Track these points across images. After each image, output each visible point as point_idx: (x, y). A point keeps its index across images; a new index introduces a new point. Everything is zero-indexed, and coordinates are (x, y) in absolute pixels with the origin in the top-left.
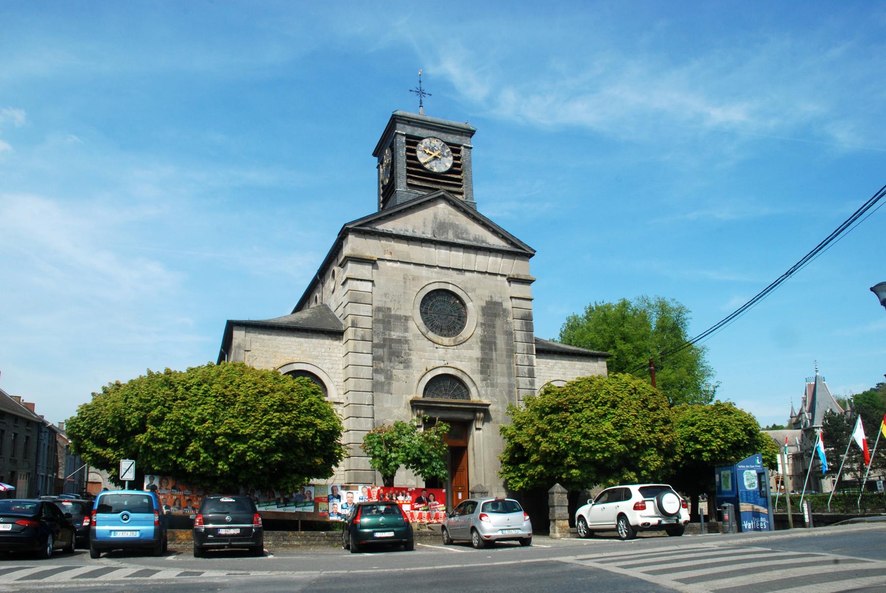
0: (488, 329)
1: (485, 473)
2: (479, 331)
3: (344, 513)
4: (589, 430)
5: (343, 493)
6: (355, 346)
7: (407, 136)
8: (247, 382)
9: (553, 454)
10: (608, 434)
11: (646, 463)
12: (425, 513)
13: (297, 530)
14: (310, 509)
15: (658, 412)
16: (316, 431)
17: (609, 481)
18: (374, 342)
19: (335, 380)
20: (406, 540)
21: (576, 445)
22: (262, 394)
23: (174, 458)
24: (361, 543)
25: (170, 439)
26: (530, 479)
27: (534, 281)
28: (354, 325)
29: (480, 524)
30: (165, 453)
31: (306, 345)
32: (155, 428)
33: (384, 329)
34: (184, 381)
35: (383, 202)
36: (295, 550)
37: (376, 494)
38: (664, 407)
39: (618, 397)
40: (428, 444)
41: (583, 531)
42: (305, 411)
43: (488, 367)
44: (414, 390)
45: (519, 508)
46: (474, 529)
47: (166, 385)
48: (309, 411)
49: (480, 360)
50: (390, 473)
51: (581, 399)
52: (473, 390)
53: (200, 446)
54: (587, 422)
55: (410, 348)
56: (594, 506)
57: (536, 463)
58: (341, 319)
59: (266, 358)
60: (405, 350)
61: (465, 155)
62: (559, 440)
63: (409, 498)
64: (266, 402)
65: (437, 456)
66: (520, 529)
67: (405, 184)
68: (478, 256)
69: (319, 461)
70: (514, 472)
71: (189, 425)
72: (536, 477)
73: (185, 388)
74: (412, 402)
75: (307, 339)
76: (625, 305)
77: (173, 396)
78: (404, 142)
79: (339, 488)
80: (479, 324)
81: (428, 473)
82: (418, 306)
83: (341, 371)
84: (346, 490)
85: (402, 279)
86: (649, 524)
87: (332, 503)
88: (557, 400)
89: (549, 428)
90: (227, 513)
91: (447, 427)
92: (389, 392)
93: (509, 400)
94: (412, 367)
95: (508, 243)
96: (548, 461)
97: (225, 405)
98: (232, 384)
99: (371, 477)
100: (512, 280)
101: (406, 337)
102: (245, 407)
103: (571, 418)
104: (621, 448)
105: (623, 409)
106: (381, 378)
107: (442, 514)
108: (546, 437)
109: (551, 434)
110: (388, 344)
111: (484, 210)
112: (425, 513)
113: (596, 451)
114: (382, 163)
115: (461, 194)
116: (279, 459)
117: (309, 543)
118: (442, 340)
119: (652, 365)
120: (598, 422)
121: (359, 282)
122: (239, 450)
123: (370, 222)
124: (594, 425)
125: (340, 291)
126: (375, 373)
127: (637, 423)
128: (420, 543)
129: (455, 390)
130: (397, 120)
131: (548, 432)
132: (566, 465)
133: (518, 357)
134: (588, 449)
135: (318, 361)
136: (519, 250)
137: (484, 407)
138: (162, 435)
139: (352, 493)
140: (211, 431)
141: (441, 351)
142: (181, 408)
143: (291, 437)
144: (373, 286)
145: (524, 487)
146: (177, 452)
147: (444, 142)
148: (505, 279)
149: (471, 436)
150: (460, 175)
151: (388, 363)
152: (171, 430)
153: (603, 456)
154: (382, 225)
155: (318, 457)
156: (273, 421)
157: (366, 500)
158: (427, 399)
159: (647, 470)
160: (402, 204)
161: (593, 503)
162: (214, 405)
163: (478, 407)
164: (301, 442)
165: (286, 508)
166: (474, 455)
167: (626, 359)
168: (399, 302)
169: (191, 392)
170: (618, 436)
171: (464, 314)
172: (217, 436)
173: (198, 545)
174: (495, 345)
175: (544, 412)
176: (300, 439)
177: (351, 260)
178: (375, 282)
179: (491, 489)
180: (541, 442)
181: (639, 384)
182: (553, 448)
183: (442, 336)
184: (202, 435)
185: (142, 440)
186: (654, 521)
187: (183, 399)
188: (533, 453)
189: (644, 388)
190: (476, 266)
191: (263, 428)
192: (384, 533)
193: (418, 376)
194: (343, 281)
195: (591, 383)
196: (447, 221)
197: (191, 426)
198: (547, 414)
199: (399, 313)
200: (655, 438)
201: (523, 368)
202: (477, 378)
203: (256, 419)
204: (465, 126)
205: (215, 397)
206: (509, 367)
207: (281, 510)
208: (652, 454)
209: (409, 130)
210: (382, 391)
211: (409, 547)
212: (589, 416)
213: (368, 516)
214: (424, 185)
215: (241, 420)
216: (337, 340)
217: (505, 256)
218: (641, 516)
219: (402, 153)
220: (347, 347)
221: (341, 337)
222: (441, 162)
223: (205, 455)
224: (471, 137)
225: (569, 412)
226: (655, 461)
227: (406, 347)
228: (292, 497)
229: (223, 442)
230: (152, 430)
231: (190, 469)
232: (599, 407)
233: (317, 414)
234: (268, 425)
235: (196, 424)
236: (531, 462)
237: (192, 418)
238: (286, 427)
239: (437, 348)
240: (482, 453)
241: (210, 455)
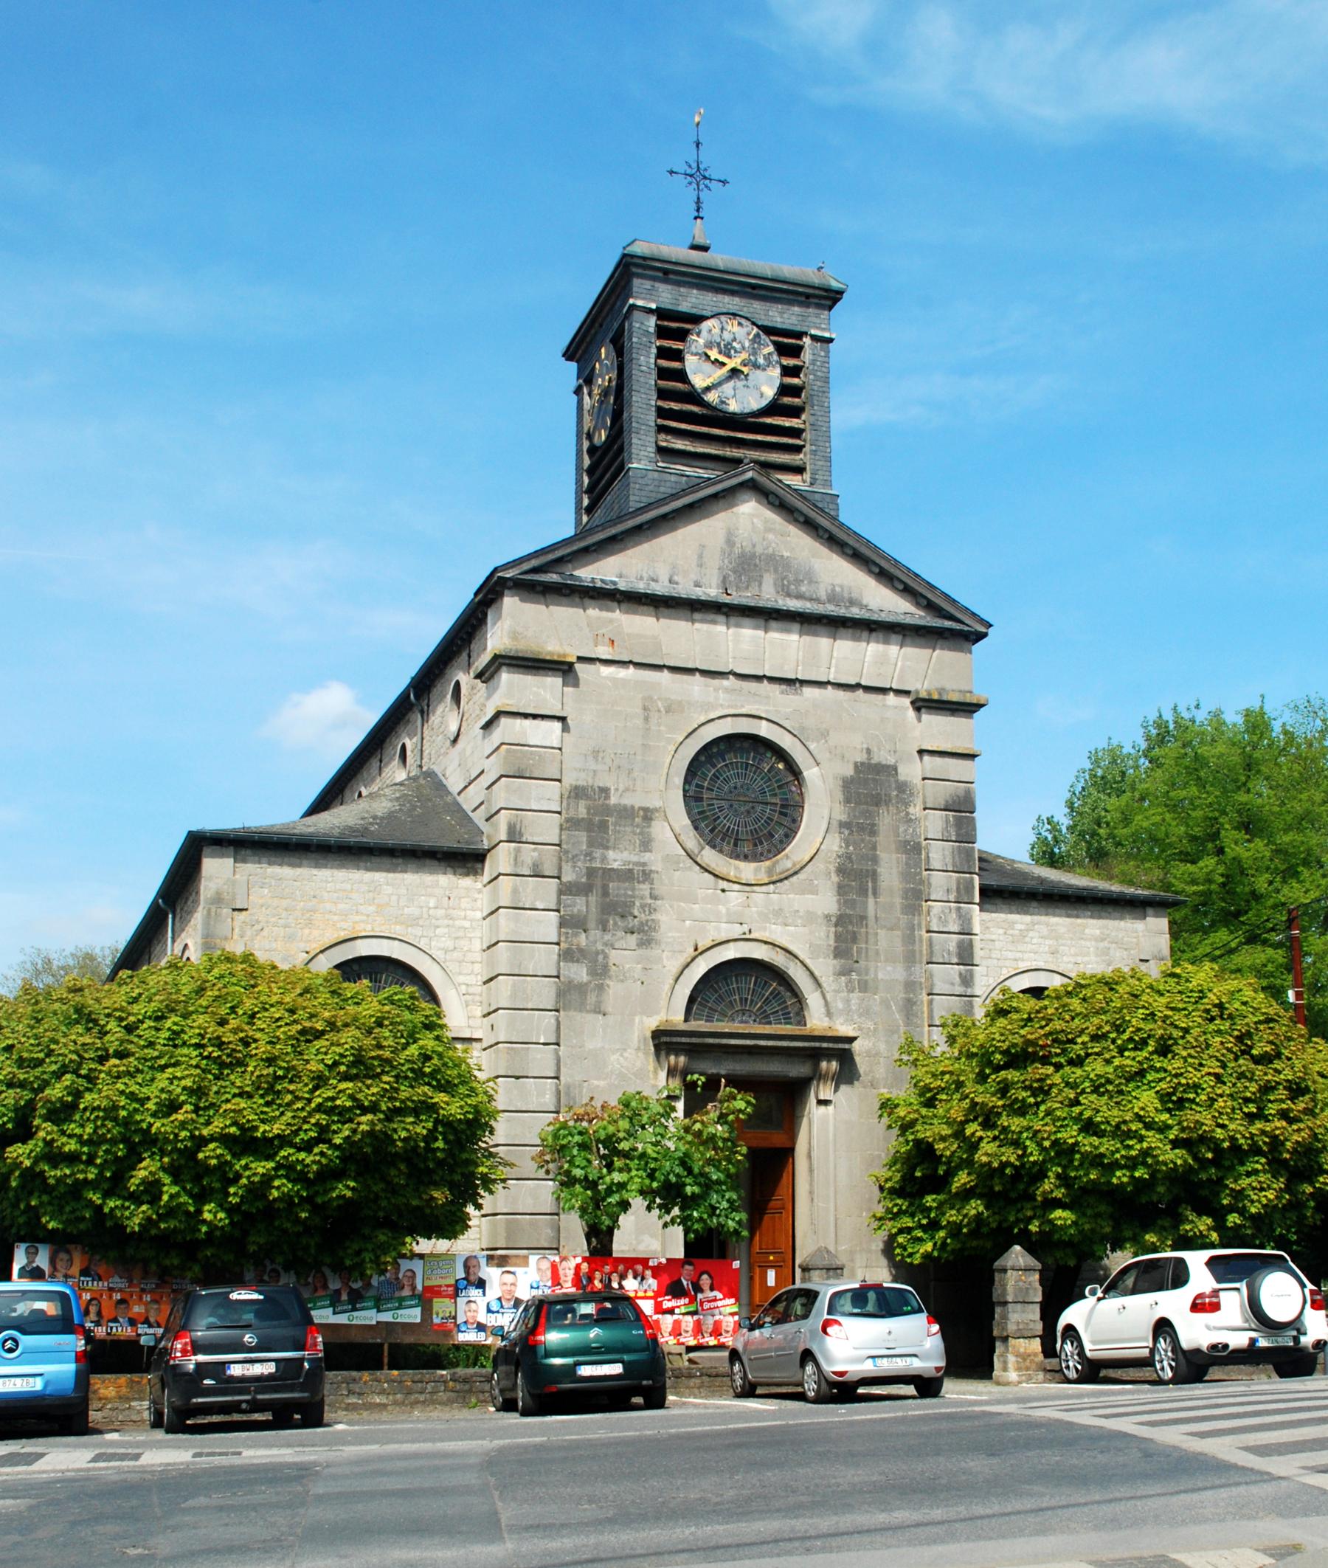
0: (856, 837)
1: (836, 1220)
2: (834, 844)
3: (494, 1323)
4: (1098, 1111)
5: (492, 1274)
6: (515, 891)
7: (661, 313)
8: (272, 1006)
9: (1008, 1171)
10: (1145, 1123)
11: (1239, 1195)
12: (689, 1322)
13: (379, 1367)
14: (413, 1315)
15: (1278, 1065)
16: (437, 1122)
17: (1147, 1237)
18: (564, 879)
19: (461, 979)
20: (651, 1382)
21: (1064, 1152)
22: (312, 1035)
23: (96, 1198)
24: (547, 1390)
25: (89, 1154)
26: (950, 1235)
27: (982, 706)
28: (514, 836)
29: (822, 1343)
30: (77, 1189)
31: (389, 890)
32: (55, 1128)
33: (591, 843)
34: (122, 1009)
35: (590, 491)
36: (385, 1416)
37: (571, 1273)
38: (1293, 1053)
39: (1176, 1027)
40: (701, 1148)
41: (1072, 1366)
42: (410, 1075)
43: (854, 939)
44: (663, 1003)
45: (915, 1304)
46: (807, 1356)
47: (77, 1022)
48: (419, 1074)
49: (834, 919)
50: (606, 1221)
51: (1082, 1032)
52: (813, 1000)
53: (163, 1168)
54: (1096, 1090)
55: (656, 892)
56: (1102, 1302)
57: (967, 1194)
58: (478, 817)
59: (286, 926)
60: (642, 898)
61: (813, 362)
62: (1025, 1135)
63: (652, 1283)
64: (320, 1057)
65: (722, 1177)
66: (915, 1355)
67: (652, 449)
68: (839, 642)
69: (440, 1195)
70: (912, 1215)
71: (138, 1118)
72: (965, 1230)
73: (125, 1027)
74: (657, 1034)
75: (391, 875)
76: (1257, 723)
77: (98, 1049)
78: (652, 330)
79: (483, 1262)
80: (835, 824)
81: (701, 1219)
82: (679, 780)
83: (478, 956)
84: (499, 1265)
85: (639, 711)
86: (1226, 1346)
87: (466, 1300)
88: (1023, 1032)
89: (1000, 1103)
90: (247, 1327)
91: (748, 1103)
92: (599, 1010)
93: (907, 1025)
94: (658, 943)
95: (918, 605)
96: (997, 1189)
97: (223, 1065)
98: (236, 1013)
99: (549, 1232)
100: (924, 705)
101: (644, 864)
102: (271, 1070)
103: (1057, 1079)
104: (1177, 1157)
105: (1185, 1059)
106: (579, 973)
107: (729, 1322)
108: (993, 1126)
109: (1004, 1121)
110: (598, 882)
111: (853, 516)
112: (689, 1322)
113: (1115, 1165)
114: (589, 381)
115: (799, 470)
116: (349, 1194)
117: (410, 1399)
118: (737, 868)
119: (1295, 924)
120: (1121, 1092)
121: (528, 722)
122: (255, 1174)
123: (560, 560)
124: (1111, 1098)
125: (476, 748)
126: (566, 960)
127: (1221, 1096)
128: (677, 1394)
129: (767, 1001)
130: (634, 270)
131: (999, 1115)
132: (1039, 1198)
133: (934, 912)
134: (1096, 1160)
135: (418, 931)
136: (948, 624)
137: (841, 1046)
138: (72, 1146)
139: (513, 1273)
140: (191, 1132)
141: (735, 898)
142: (118, 1077)
143: (379, 1139)
144: (563, 730)
145: (936, 1254)
146: (106, 1186)
147: (758, 327)
148: (906, 701)
149: (805, 1122)
150: (798, 417)
151: (599, 933)
152: (95, 1131)
153: (1132, 1177)
154: (590, 568)
155: (437, 1185)
156: (338, 1102)
157: (546, 1291)
158: (698, 1025)
159: (1242, 1212)
160: (648, 507)
161: (1100, 1294)
162: (197, 1066)
163: (825, 1045)
164: (401, 1151)
165: (355, 1314)
166: (811, 1170)
167: (1251, 884)
168: (630, 771)
169: (140, 1037)
170: (1170, 1127)
171: (797, 798)
172: (201, 1142)
173: (178, 1403)
174: (875, 880)
175: (990, 1063)
176: (399, 1144)
177: (509, 665)
178: (569, 721)
179: (852, 1260)
180: (981, 1138)
181: (1232, 993)
182: (1010, 1155)
183: (737, 857)
184: (167, 1140)
185: (21, 1159)
186: (1239, 1340)
187: (121, 1055)
188: (959, 1168)
189: (1245, 1003)
190: (833, 670)
191: (313, 1121)
192: (599, 1367)
193: (673, 966)
194: (487, 718)
195: (1112, 989)
196: (759, 550)
197: (143, 1121)
198: (998, 1069)
199: (628, 801)
200: (1263, 1132)
201: (946, 941)
202: (825, 967)
203: (298, 1098)
204: (816, 280)
205: (198, 1046)
206: (910, 939)
207: (342, 1319)
208: (1256, 1172)
209: (665, 296)
210: (582, 1008)
211: (655, 1400)
212: (1099, 1076)
213: (562, 1328)
214: (702, 448)
215: (261, 1101)
216: (467, 875)
217: (908, 640)
218: (1208, 1328)
219: (645, 362)
220: (495, 894)
221: (479, 866)
222: (750, 383)
223: (175, 1189)
224: (830, 308)
225: (1051, 1064)
226: (1262, 1189)
227: (644, 889)
228: (368, 1285)
229: (218, 1157)
230: (48, 1133)
231: (135, 1224)
232: (1126, 1054)
233: (438, 1081)
234: (325, 1112)
235: (154, 1115)
236: (954, 1191)
237: (143, 1101)
238: (370, 1117)
239: (723, 891)
240: (832, 1166)
241: (184, 1189)
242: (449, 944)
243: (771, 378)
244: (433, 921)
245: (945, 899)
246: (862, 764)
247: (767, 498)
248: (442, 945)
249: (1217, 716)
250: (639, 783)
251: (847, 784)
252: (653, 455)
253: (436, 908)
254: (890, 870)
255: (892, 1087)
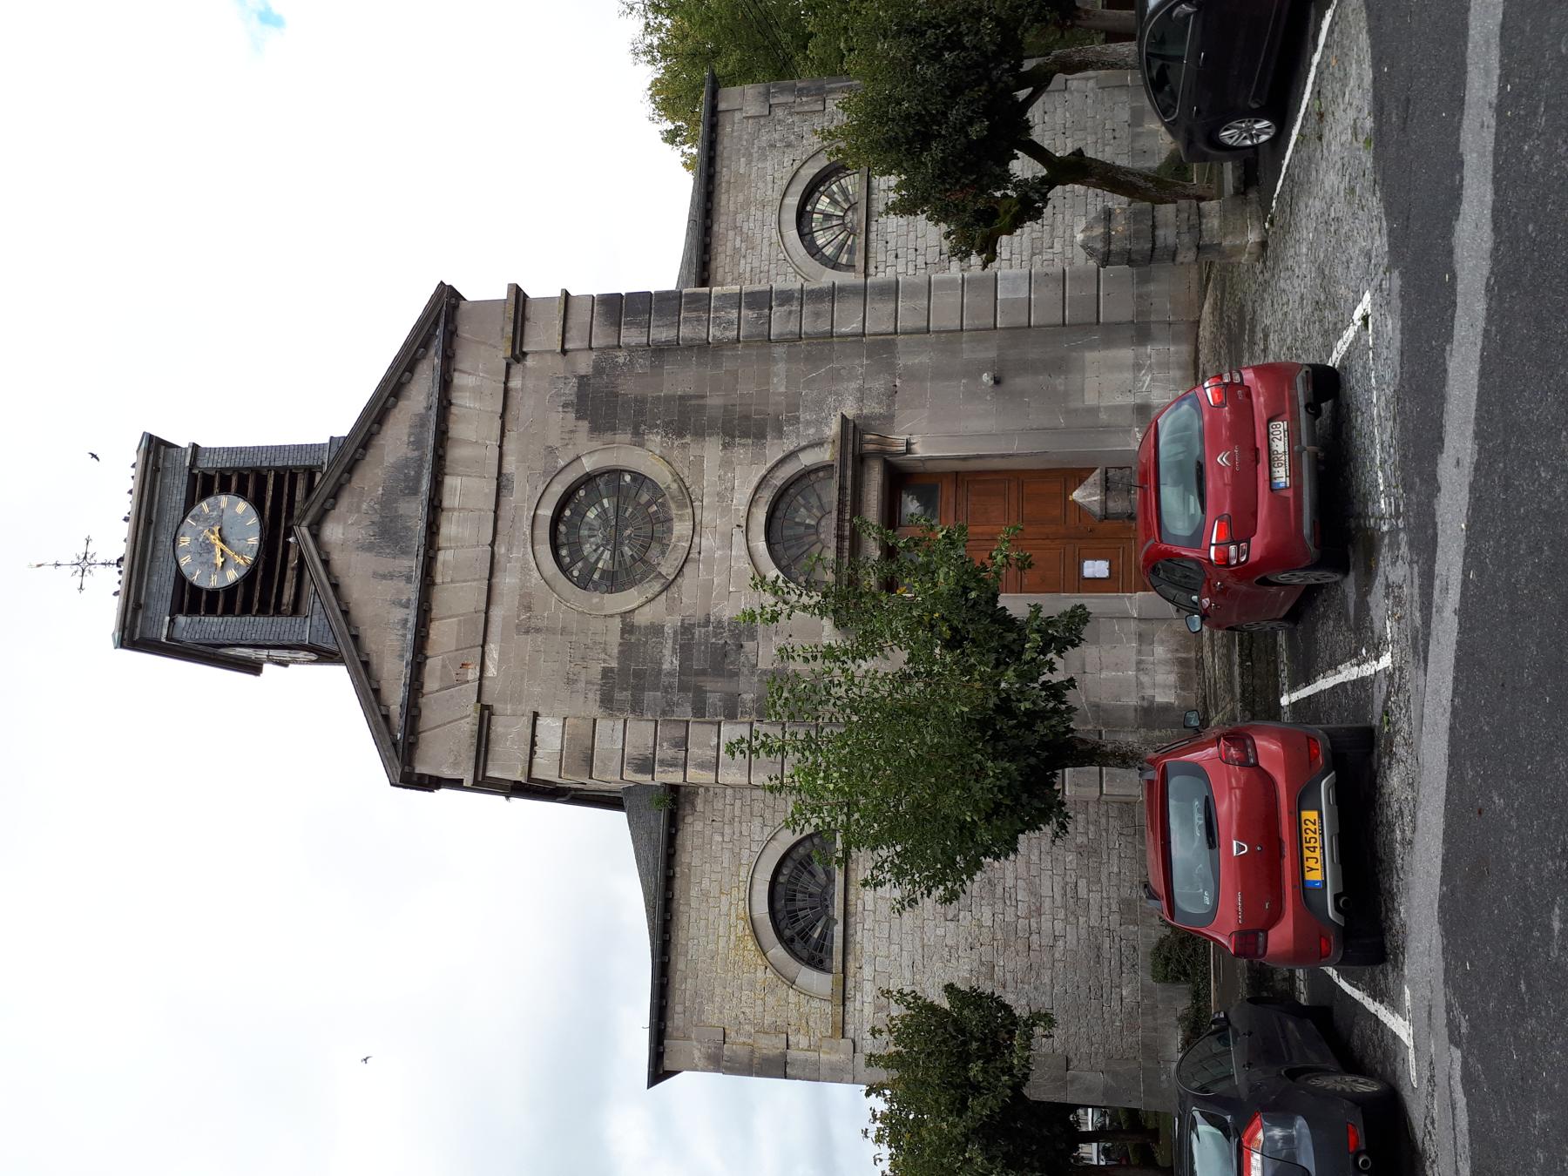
31: (706, 883)
33: (656, 689)
43: (747, 417)
52: (808, 459)
60: (707, 635)
85: (529, 637)
95: (424, 357)
101: (675, 632)
135: (745, 853)
141: (707, 542)
174: (691, 397)
196: (376, 518)
199: (615, 651)
242: (757, 822)
243: (230, 504)
244: (735, 837)
245: (706, 323)
246: (577, 411)
247: (329, 510)
248: (759, 829)
249: (947, 236)
250: (598, 638)
251: (595, 429)
252: (298, 619)
253: (723, 836)
254: (679, 380)
255: (895, 374)
